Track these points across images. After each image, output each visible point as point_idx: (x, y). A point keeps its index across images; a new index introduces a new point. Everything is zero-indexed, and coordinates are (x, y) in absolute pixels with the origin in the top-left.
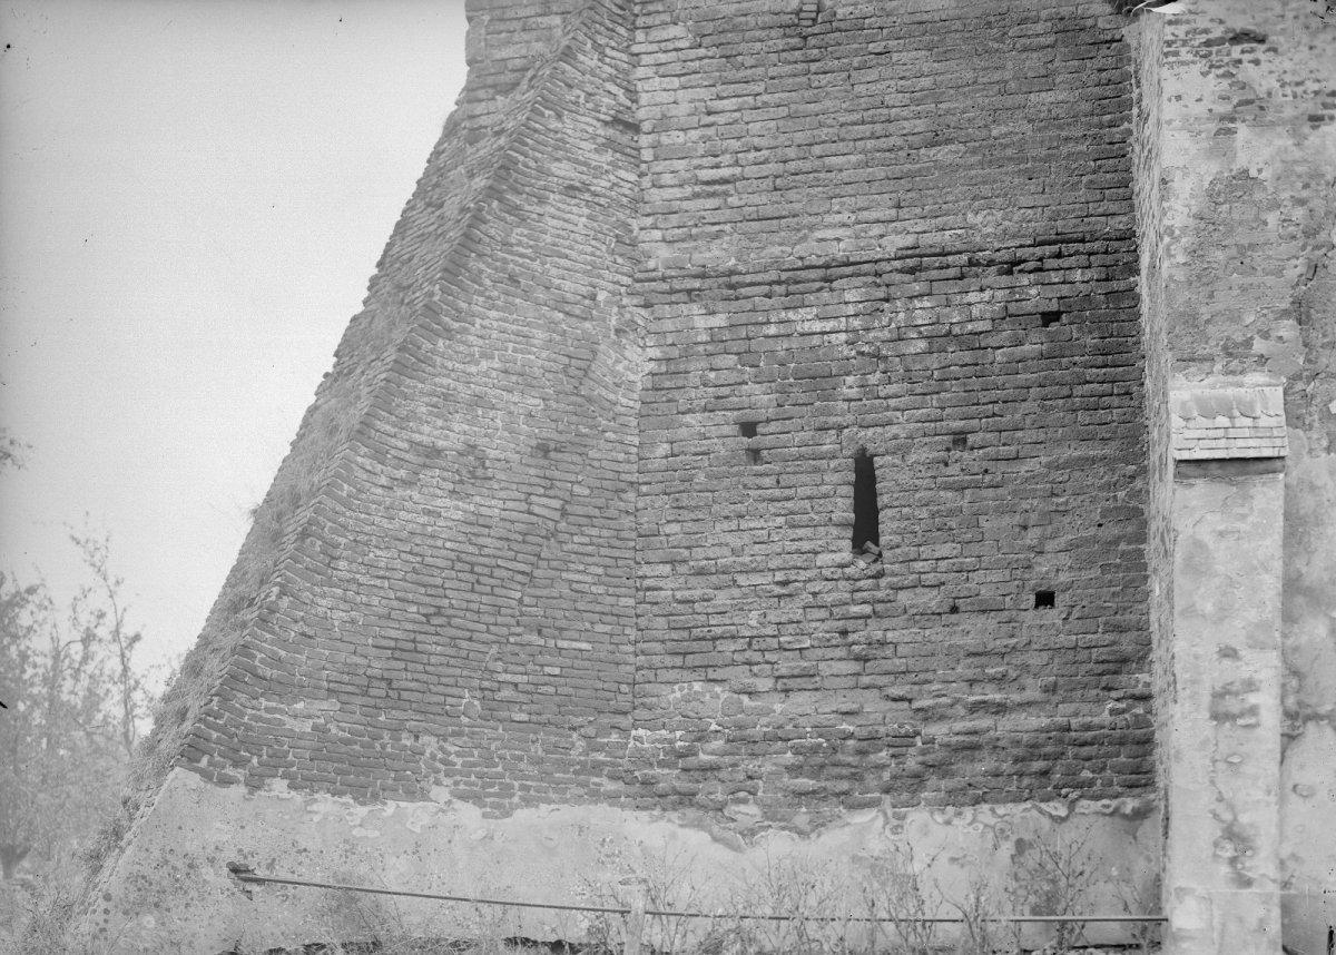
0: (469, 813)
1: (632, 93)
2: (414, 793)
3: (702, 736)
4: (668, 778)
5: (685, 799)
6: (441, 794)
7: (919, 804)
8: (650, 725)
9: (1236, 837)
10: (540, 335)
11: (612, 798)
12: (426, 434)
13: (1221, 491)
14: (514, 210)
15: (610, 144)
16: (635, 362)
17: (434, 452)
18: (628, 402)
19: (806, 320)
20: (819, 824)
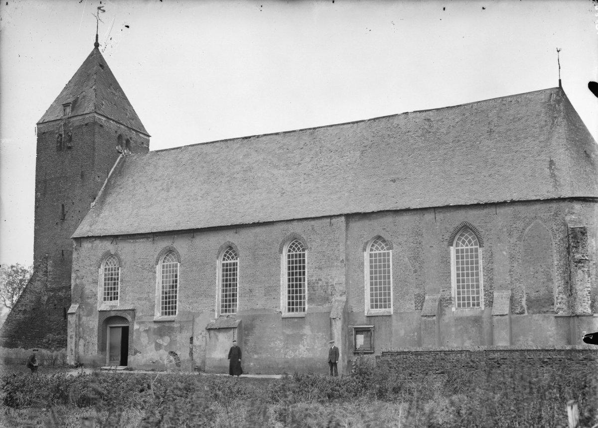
0: (23, 350)
1: (47, 268)
2: (17, 347)
3: (49, 340)
4: (46, 345)
5: (48, 348)
6: (20, 347)
7: (384, 354)
8: (45, 339)
9: (72, 350)
10: (34, 297)
11: (41, 348)
12: (20, 309)
13: (71, 316)
14: (32, 283)
15: (44, 275)
16: (46, 298)
17: (21, 311)
18: (44, 303)
19: (60, 294)
20: (59, 350)
